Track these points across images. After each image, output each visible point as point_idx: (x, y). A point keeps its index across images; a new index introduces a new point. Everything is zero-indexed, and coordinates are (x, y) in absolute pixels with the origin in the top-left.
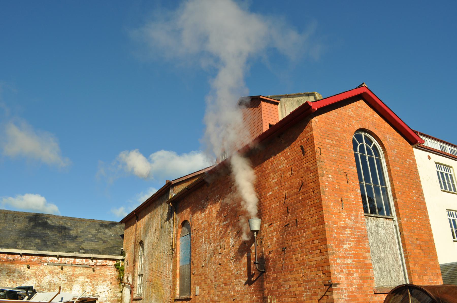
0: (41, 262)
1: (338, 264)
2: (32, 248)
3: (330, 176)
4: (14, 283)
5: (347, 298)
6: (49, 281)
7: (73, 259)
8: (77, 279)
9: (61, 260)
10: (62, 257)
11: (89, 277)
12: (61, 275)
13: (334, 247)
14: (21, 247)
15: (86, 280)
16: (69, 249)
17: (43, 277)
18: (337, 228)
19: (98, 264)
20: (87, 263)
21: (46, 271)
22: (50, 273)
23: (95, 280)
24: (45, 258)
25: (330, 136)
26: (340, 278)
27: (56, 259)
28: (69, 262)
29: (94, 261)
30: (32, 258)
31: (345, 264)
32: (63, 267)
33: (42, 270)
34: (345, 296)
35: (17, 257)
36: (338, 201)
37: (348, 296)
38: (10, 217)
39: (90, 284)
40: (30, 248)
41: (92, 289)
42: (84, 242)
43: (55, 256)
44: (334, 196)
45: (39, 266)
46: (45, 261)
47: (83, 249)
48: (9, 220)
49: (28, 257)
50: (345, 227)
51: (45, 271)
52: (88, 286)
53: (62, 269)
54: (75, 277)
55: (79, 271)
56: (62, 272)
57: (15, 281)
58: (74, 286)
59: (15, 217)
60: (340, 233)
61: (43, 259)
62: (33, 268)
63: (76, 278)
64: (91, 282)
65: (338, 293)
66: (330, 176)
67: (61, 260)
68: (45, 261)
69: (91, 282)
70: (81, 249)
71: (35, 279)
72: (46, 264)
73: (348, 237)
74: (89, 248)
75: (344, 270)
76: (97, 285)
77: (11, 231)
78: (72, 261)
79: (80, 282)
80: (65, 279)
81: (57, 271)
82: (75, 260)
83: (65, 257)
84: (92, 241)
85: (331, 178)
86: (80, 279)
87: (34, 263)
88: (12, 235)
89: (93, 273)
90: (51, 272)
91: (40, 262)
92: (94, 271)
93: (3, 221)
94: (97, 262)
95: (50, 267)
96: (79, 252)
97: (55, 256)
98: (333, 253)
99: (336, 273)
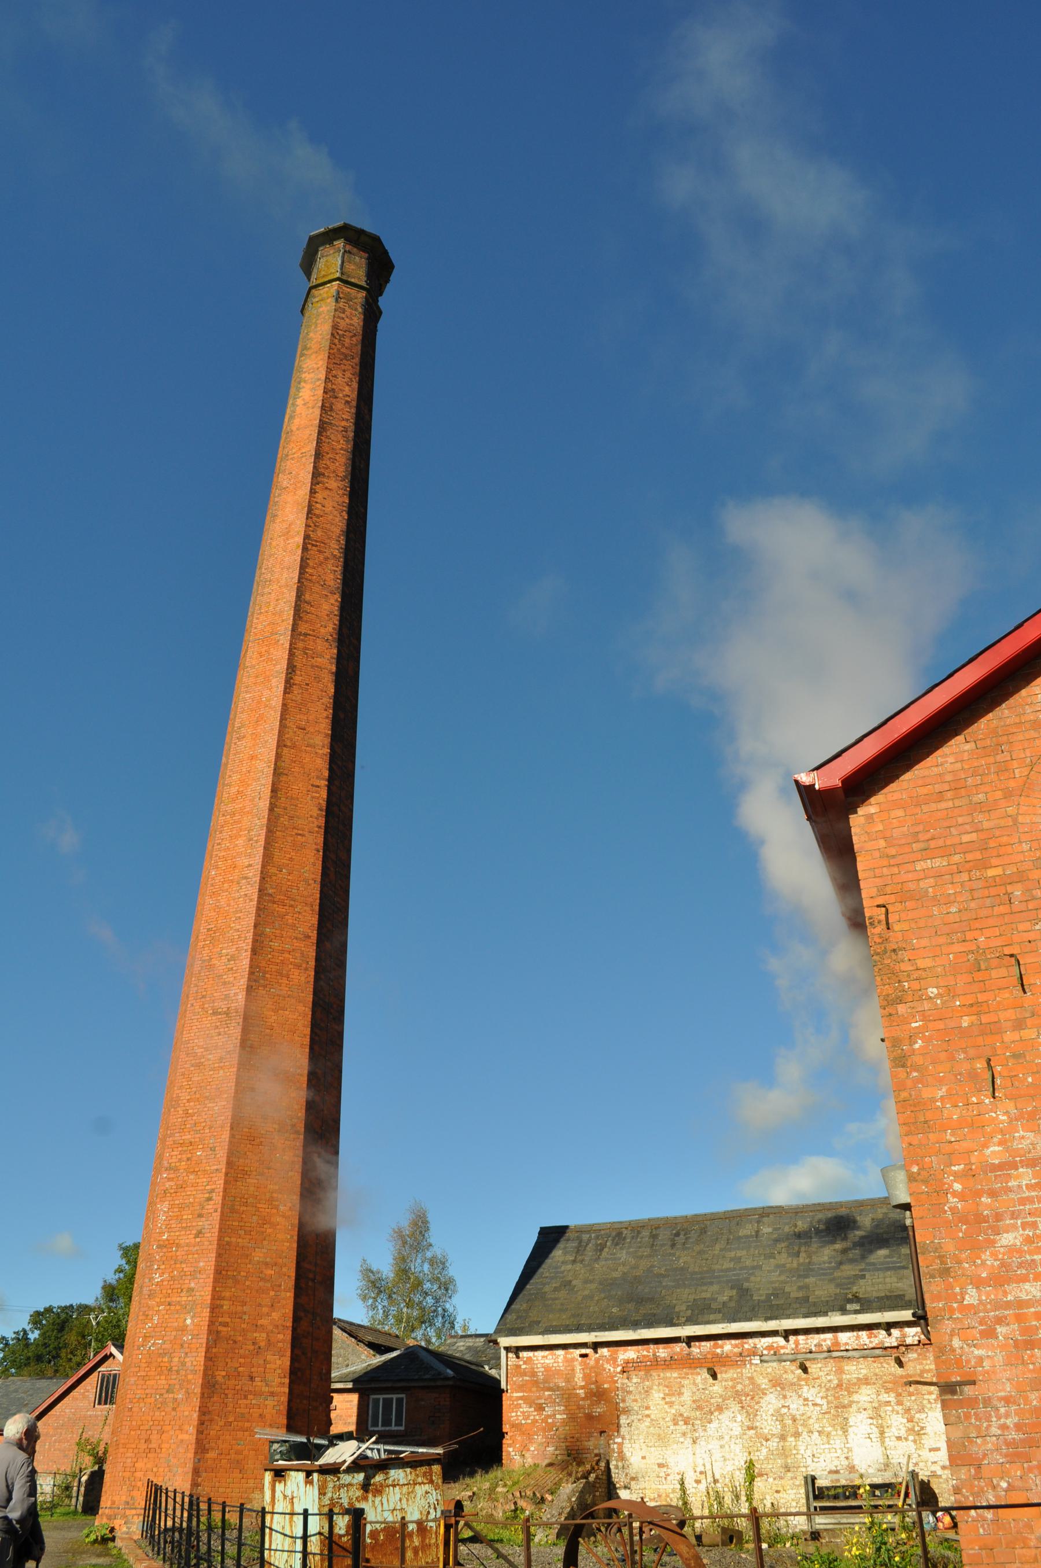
0: (743, 1357)
1: (966, 1309)
2: (712, 1317)
3: (933, 991)
4: (686, 1423)
5: (1013, 1435)
6: (778, 1411)
7: (829, 1336)
8: (855, 1397)
9: (797, 1343)
10: (796, 1332)
11: (890, 1386)
12: (806, 1388)
13: (949, 1247)
14: (683, 1319)
15: (884, 1397)
16: (815, 1304)
17: (757, 1398)
18: (969, 1174)
19: (909, 1341)
20: (875, 1342)
21: (763, 1382)
22: (774, 1386)
23: (911, 1394)
24: (751, 1341)
25: (933, 844)
26: (980, 1360)
27: (780, 1341)
28: (818, 1345)
29: (896, 1332)
30: (716, 1346)
31: (1008, 1305)
32: (808, 1364)
33: (751, 1379)
34: (1004, 1427)
35: (678, 1348)
36: (973, 1075)
37: (1018, 1427)
38: (664, 1235)
39: (899, 1408)
40: (706, 1317)
41: (910, 1425)
42: (863, 1277)
43: (774, 1333)
44: (952, 1058)
45: (740, 1366)
46: (754, 1352)
47: (856, 1299)
48: (662, 1245)
49: (707, 1345)
50: (1008, 1166)
51: (759, 1382)
52: (894, 1416)
53: (805, 1370)
54: (847, 1390)
55: (854, 1370)
56: (806, 1380)
57: (689, 1418)
58: (852, 1421)
59: (677, 1234)
60: (979, 1194)
61: (746, 1346)
62: (726, 1375)
63: (850, 1393)
64: (899, 1403)
65: (967, 1416)
66: (933, 991)
67: (797, 1343)
68: (754, 1352)
69: (899, 1403)
70: (850, 1301)
71: (737, 1407)
72: (756, 1360)
73: (1023, 1201)
74: (875, 1294)
75: (1001, 1330)
76: (921, 1410)
77: (664, 1276)
78: (829, 1343)
79: (868, 1406)
80: (819, 1401)
81: (790, 1376)
82: (836, 1338)
83: (807, 1331)
84: (888, 1269)
85: (939, 995)
86: (865, 1396)
87: (726, 1361)
88: (664, 1287)
89: (900, 1371)
90: (776, 1383)
91: (741, 1354)
92: (900, 1363)
93: (647, 1251)
94: (904, 1336)
95: (772, 1367)
96: (844, 1311)
97: (774, 1333)
98: (945, 1272)
99: (956, 1343)
